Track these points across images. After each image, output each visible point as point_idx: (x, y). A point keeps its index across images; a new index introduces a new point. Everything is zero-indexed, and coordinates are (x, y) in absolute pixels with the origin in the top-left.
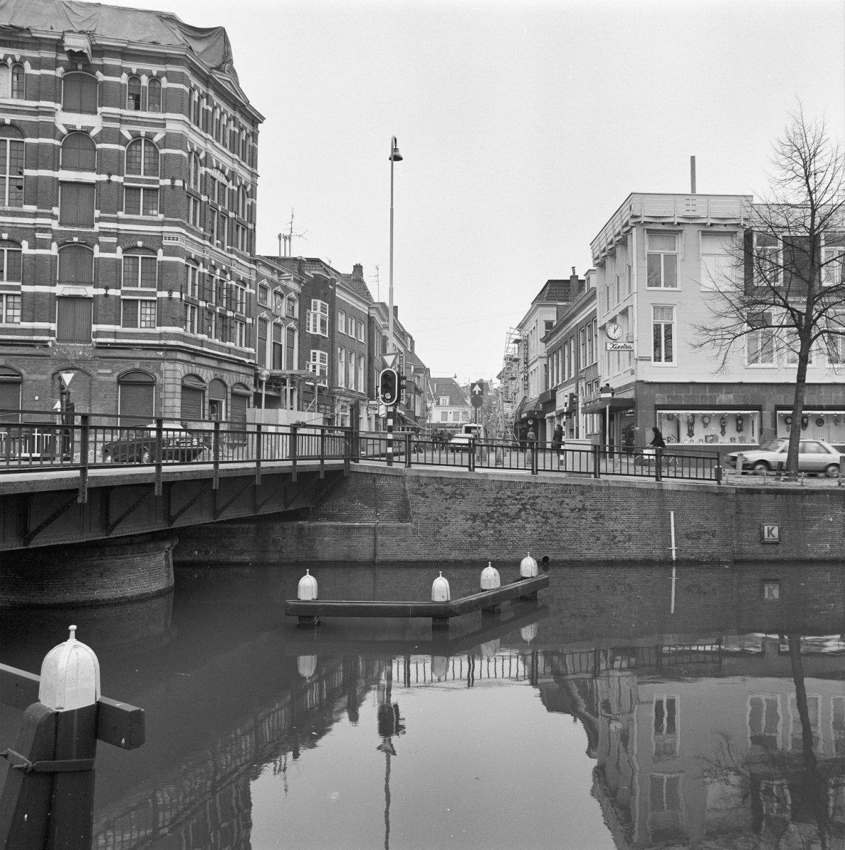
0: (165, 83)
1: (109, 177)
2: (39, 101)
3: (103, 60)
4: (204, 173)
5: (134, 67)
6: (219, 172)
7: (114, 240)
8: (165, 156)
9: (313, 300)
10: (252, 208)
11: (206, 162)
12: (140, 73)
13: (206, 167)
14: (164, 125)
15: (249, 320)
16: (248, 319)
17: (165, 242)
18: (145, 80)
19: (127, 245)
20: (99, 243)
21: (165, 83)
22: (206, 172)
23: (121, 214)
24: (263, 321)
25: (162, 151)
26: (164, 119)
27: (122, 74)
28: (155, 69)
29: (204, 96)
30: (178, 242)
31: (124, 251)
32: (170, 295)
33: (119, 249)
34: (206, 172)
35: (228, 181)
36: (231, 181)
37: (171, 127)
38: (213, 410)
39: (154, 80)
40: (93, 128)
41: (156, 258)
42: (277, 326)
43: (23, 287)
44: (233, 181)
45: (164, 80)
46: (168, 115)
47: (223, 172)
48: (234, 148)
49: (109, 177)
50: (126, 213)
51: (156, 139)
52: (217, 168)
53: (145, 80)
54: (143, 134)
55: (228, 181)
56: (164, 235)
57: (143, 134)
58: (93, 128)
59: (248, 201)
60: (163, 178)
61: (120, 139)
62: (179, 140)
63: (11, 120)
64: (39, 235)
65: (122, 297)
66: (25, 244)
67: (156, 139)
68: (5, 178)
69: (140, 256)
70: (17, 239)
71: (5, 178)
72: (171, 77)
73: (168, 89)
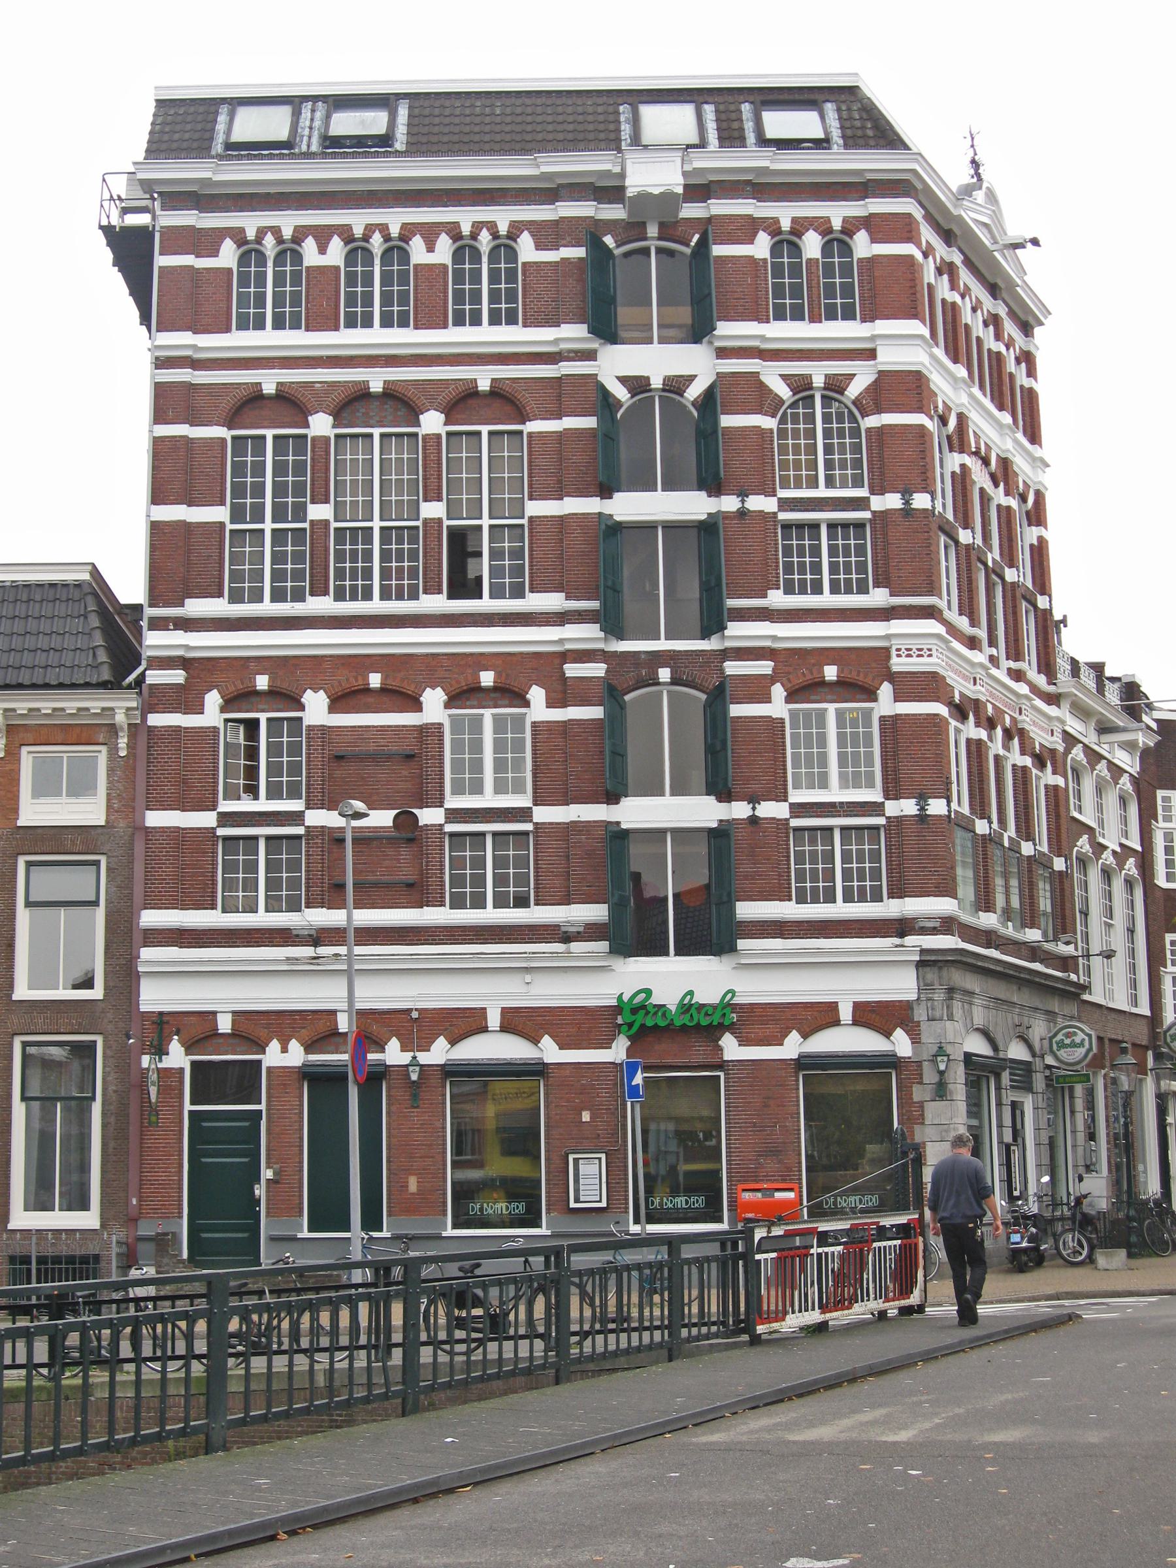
0: (863, 246)
1: (743, 501)
2: (557, 324)
3: (708, 207)
4: (958, 470)
5: (785, 213)
6: (980, 462)
7: (765, 667)
8: (882, 431)
9: (1160, 794)
10: (1040, 552)
11: (959, 441)
12: (800, 227)
13: (962, 452)
14: (871, 354)
15: (1059, 864)
16: (1056, 860)
17: (898, 664)
18: (812, 246)
19: (799, 681)
20: (892, 677)
21: (863, 246)
22: (963, 466)
23: (777, 599)
24: (1083, 862)
25: (872, 421)
26: (873, 338)
27: (755, 235)
28: (837, 213)
29: (945, 268)
30: (933, 660)
31: (228, 704)
32: (922, 809)
33: (778, 692)
34: (963, 466)
35: (996, 485)
36: (1002, 484)
37: (891, 358)
38: (698, 1141)
39: (837, 242)
40: (691, 378)
41: (300, 719)
42: (1107, 874)
43: (888, 804)
44: (1006, 484)
45: (309, 247)
46: (883, 327)
47: (986, 462)
48: (1001, 394)
49: (743, 501)
50: (450, 597)
51: (854, 390)
52: (977, 453)
53: (812, 246)
54: (818, 381)
55: (996, 485)
56: (895, 644)
57: (818, 381)
58: (691, 378)
59: (1032, 534)
60: (878, 489)
61: (763, 400)
62: (907, 388)
63: (826, 376)
64: (573, 670)
65: (221, 832)
66: (537, 694)
67: (854, 390)
68: (262, 531)
69: (263, 717)
70: (515, 684)
71: (262, 531)
72: (879, 227)
73: (873, 261)
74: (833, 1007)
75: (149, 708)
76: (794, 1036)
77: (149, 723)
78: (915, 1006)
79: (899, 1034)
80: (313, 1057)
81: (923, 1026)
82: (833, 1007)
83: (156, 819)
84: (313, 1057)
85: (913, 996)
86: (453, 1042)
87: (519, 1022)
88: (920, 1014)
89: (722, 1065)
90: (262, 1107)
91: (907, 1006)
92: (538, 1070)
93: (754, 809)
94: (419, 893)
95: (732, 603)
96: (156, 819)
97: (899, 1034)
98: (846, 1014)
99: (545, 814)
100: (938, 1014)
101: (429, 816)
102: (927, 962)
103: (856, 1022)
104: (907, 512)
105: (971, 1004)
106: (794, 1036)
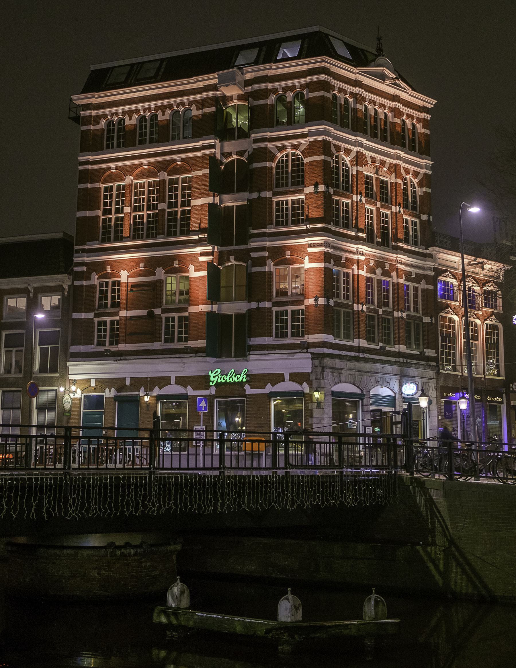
44: (395, 172)
74: (283, 375)
75: (74, 279)
76: (157, 388)
77: (75, 284)
78: (311, 374)
79: (305, 384)
80: (119, 394)
81: (313, 382)
82: (283, 375)
83: (76, 316)
84: (119, 394)
85: (310, 370)
86: (160, 389)
87: (181, 381)
88: (312, 377)
89: (245, 396)
90: (103, 410)
91: (308, 374)
92: (185, 397)
93: (259, 304)
94: (154, 337)
95: (76, 248)
96: (76, 316)
97: (305, 384)
98: (287, 377)
99: (91, 315)
100: (319, 377)
101: (157, 311)
102: (315, 357)
103: (176, 383)
104: (259, 198)
105: (339, 373)
106: (157, 388)
